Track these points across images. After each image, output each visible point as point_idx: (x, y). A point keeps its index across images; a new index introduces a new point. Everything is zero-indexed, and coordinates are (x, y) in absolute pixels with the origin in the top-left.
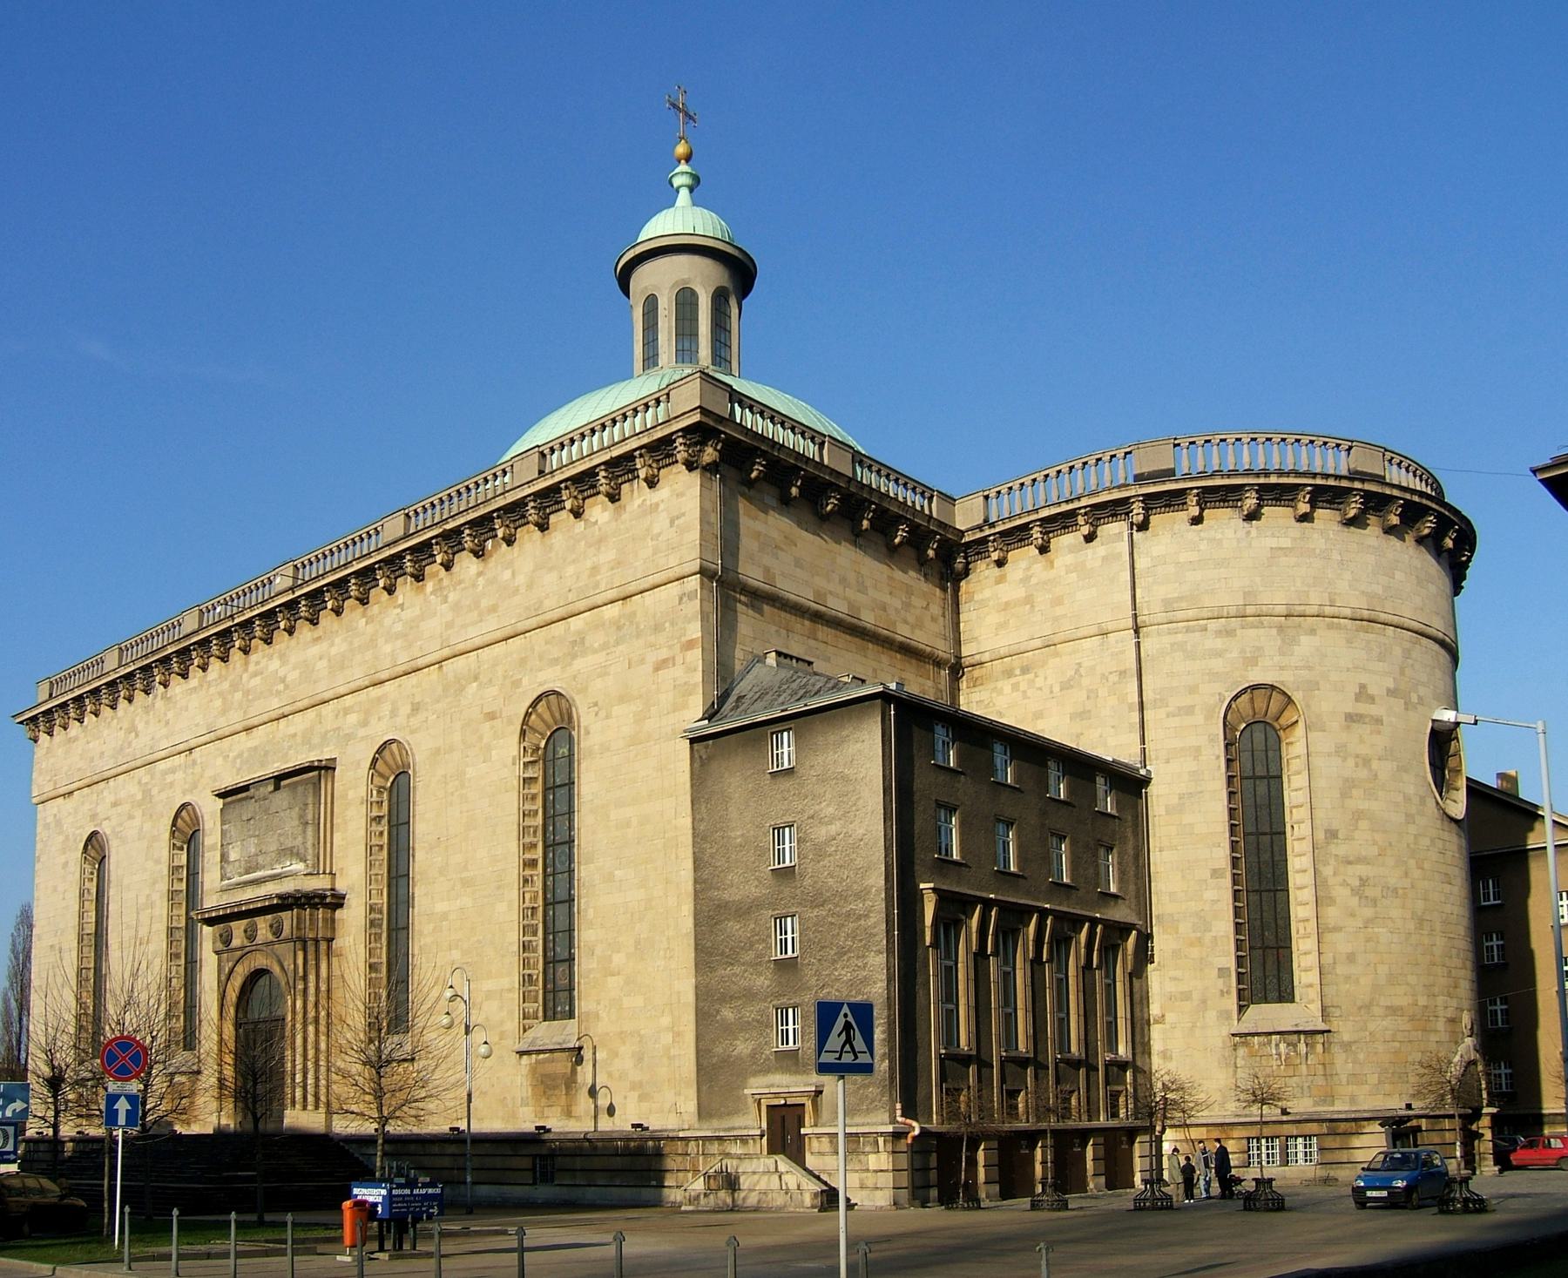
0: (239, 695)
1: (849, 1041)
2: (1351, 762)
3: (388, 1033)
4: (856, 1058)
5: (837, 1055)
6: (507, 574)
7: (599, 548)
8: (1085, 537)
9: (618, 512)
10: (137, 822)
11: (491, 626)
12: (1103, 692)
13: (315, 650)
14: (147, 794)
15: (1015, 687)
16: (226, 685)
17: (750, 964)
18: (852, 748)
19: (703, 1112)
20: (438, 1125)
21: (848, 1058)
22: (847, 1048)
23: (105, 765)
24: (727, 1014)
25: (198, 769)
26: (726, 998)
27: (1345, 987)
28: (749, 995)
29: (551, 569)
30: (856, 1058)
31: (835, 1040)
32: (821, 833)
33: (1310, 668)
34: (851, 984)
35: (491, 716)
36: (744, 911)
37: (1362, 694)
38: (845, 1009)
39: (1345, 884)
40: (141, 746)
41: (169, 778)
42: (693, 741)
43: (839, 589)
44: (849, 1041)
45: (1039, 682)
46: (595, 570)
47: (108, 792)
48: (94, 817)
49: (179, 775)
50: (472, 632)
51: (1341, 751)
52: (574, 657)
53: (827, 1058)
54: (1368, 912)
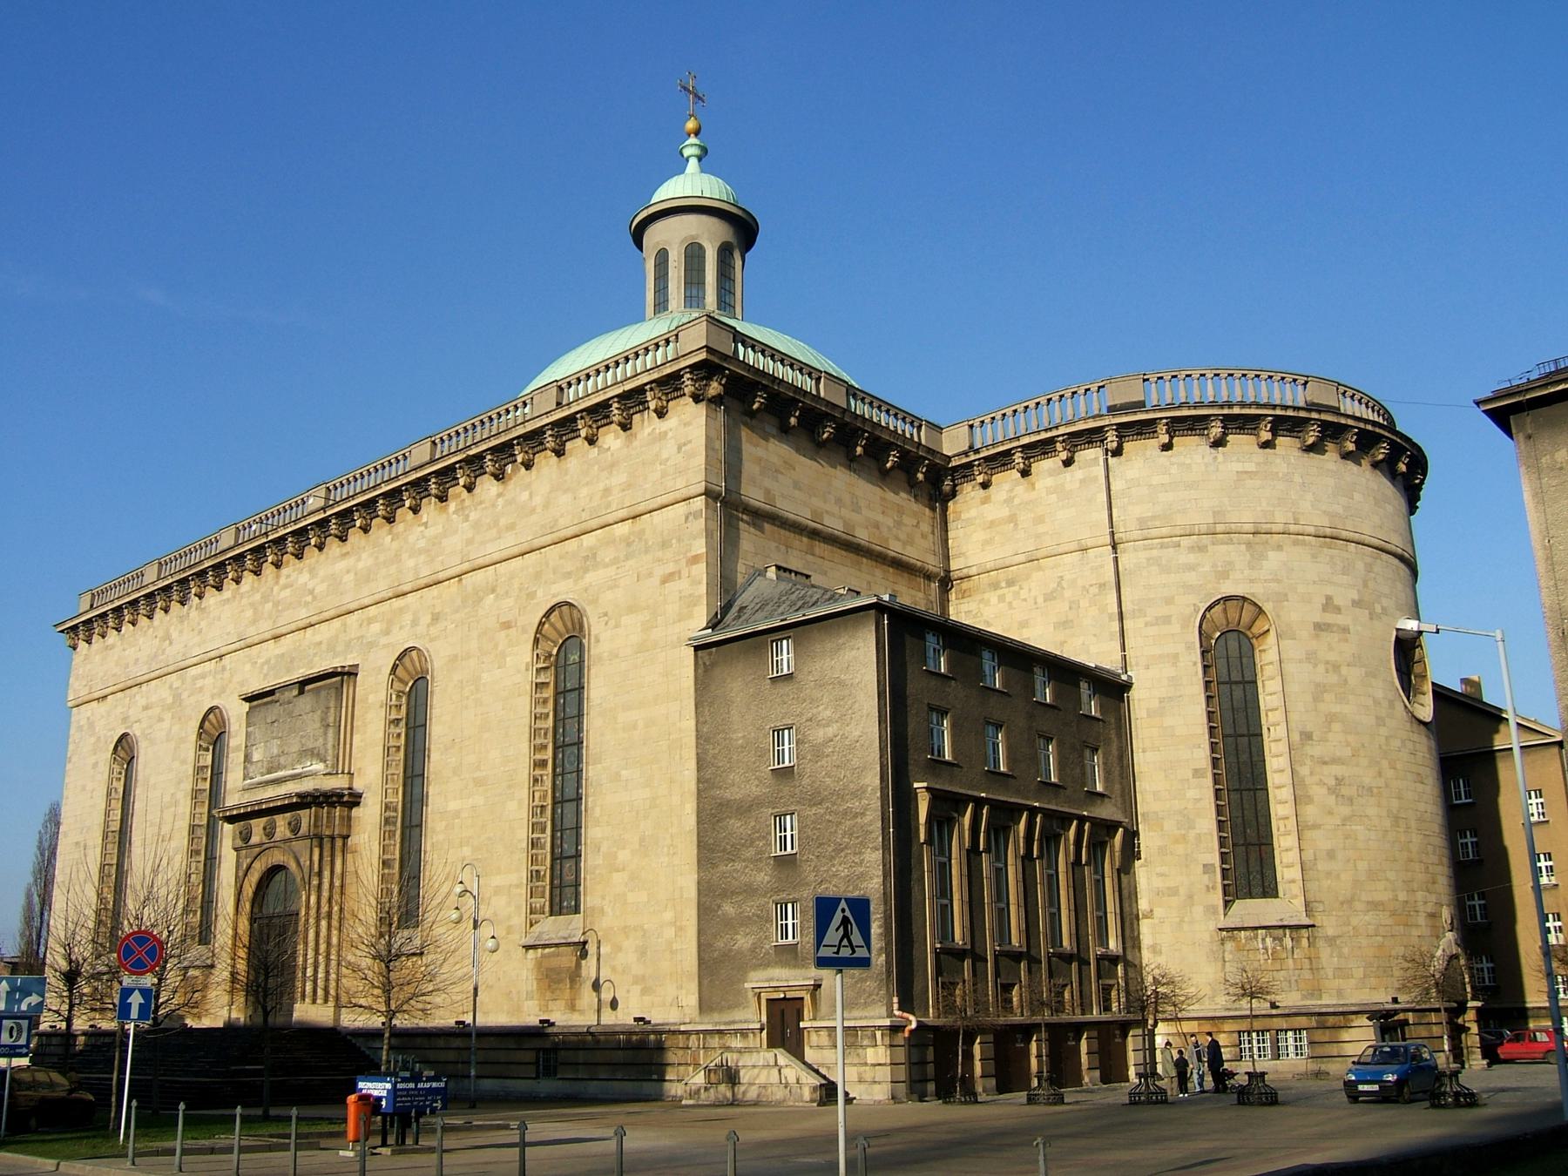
0: (269, 606)
1: (846, 935)
2: (1321, 668)
3: (398, 928)
4: (854, 952)
5: (835, 949)
6: (525, 496)
9: (629, 440)
10: (165, 725)
11: (509, 543)
12: (1084, 603)
13: (342, 565)
14: (177, 697)
15: (1001, 599)
16: (258, 597)
17: (751, 860)
18: (848, 655)
19: (705, 1006)
21: (845, 952)
22: (845, 942)
23: (139, 671)
24: (728, 909)
25: (227, 675)
26: (726, 894)
27: (1326, 883)
28: (750, 891)
29: (566, 491)
30: (854, 952)
31: (833, 935)
32: (819, 735)
33: (1278, 581)
34: (848, 880)
35: (507, 625)
36: (744, 809)
37: (1329, 605)
38: (843, 904)
39: (1321, 783)
40: (173, 653)
41: (199, 683)
42: (697, 648)
43: (835, 509)
44: (846, 935)
45: (1024, 594)
46: (607, 491)
47: (140, 697)
48: (125, 719)
49: (209, 681)
50: (490, 548)
51: (1311, 657)
52: (586, 571)
54: (1345, 810)
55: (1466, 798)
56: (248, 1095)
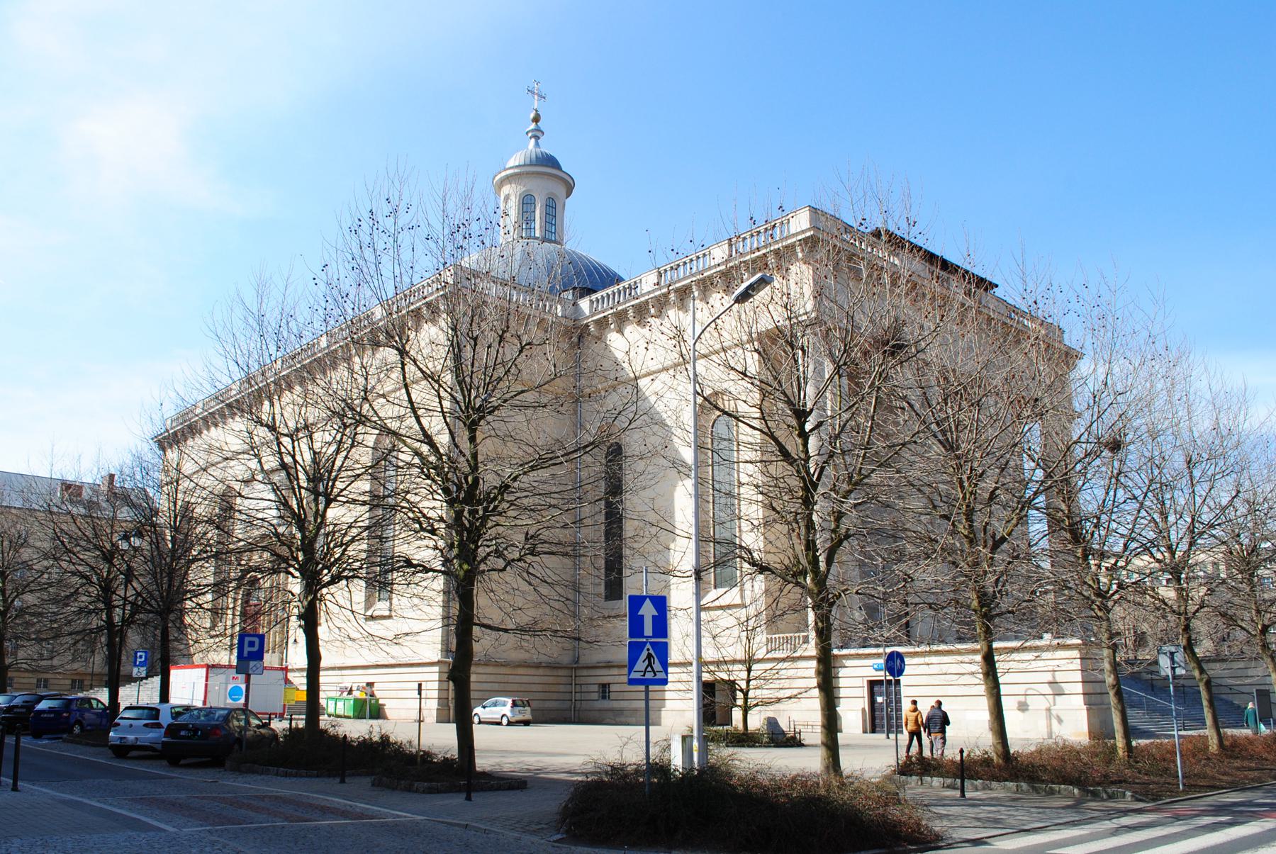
1: (650, 664)
5: (642, 674)
7: (847, 532)
8: (114, 475)
20: (996, 658)
21: (649, 675)
22: (649, 669)
30: (655, 675)
31: (641, 665)
38: (648, 646)
44: (650, 664)
53: (634, 675)
55: (1203, 724)
56: (832, 692)
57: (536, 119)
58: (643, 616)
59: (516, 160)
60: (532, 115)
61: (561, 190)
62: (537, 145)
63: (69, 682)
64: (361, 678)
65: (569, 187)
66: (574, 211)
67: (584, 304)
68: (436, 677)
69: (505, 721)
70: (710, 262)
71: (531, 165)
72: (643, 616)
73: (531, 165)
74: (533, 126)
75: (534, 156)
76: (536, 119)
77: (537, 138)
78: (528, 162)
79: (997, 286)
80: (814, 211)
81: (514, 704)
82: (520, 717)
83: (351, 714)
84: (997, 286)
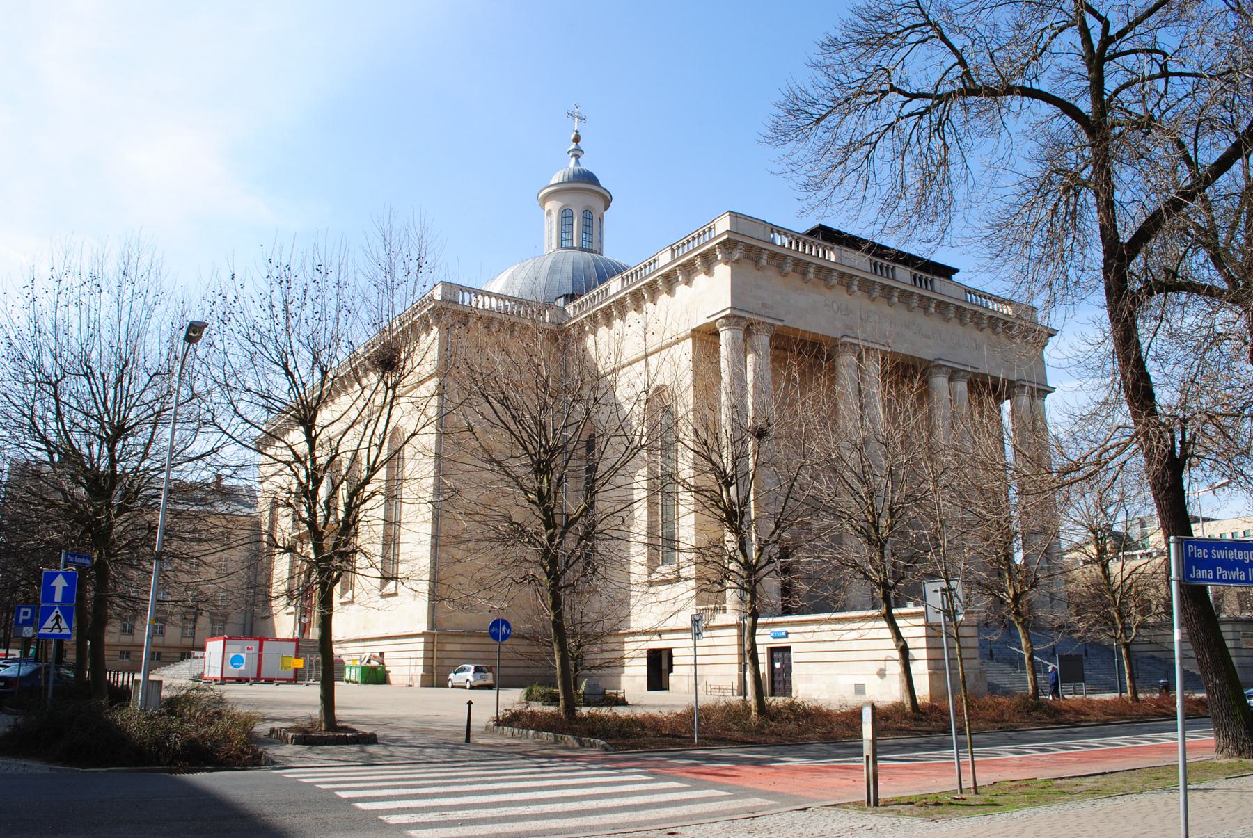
1: (57, 623)
38: (57, 609)
44: (57, 623)
57: (577, 140)
58: (54, 587)
59: (557, 178)
60: (573, 136)
61: (597, 204)
62: (577, 163)
63: (118, 653)
64: (373, 649)
65: (607, 201)
66: (612, 221)
67: (570, 309)
68: (422, 646)
69: (468, 686)
70: (660, 264)
71: (569, 182)
72: (54, 587)
73: (569, 182)
74: (573, 146)
75: (571, 173)
76: (577, 140)
77: (577, 157)
78: (566, 180)
79: (956, 271)
80: (734, 215)
81: (477, 670)
82: (481, 682)
83: (359, 679)
84: (956, 271)
